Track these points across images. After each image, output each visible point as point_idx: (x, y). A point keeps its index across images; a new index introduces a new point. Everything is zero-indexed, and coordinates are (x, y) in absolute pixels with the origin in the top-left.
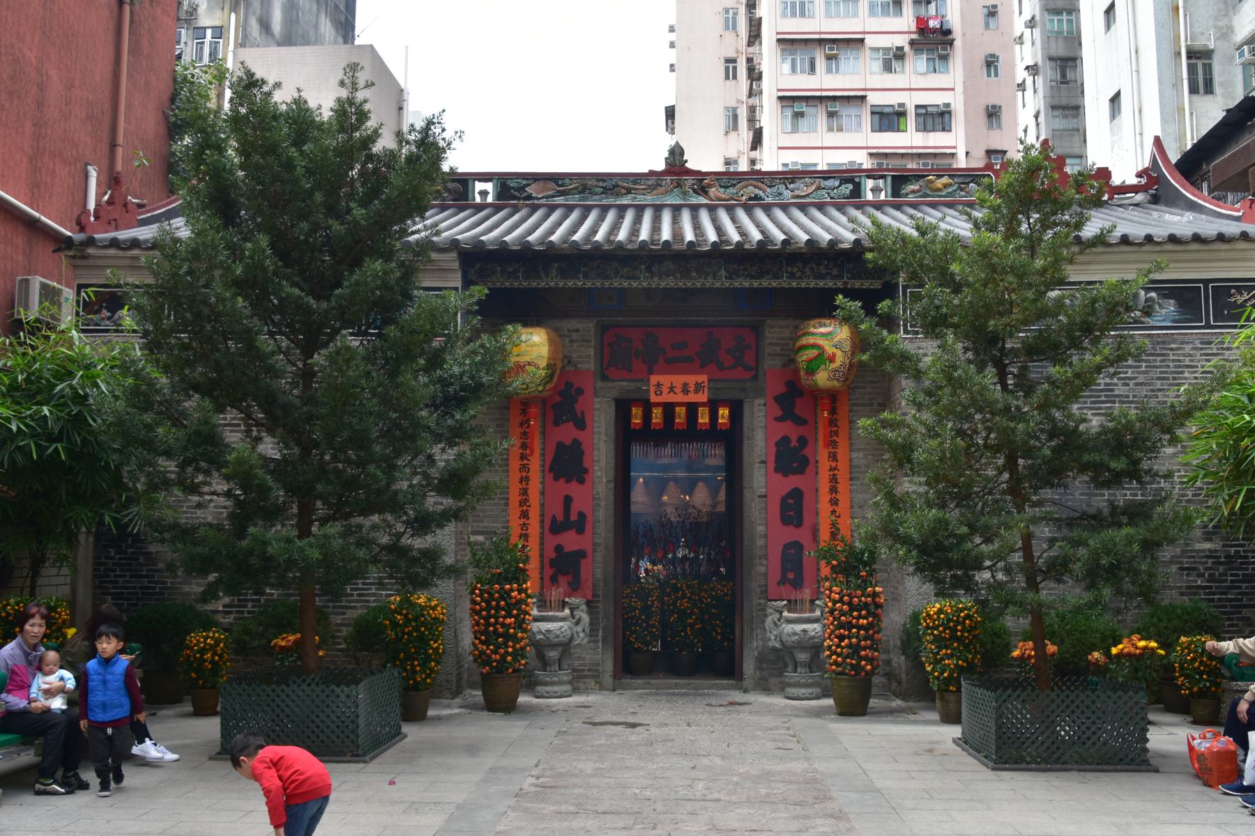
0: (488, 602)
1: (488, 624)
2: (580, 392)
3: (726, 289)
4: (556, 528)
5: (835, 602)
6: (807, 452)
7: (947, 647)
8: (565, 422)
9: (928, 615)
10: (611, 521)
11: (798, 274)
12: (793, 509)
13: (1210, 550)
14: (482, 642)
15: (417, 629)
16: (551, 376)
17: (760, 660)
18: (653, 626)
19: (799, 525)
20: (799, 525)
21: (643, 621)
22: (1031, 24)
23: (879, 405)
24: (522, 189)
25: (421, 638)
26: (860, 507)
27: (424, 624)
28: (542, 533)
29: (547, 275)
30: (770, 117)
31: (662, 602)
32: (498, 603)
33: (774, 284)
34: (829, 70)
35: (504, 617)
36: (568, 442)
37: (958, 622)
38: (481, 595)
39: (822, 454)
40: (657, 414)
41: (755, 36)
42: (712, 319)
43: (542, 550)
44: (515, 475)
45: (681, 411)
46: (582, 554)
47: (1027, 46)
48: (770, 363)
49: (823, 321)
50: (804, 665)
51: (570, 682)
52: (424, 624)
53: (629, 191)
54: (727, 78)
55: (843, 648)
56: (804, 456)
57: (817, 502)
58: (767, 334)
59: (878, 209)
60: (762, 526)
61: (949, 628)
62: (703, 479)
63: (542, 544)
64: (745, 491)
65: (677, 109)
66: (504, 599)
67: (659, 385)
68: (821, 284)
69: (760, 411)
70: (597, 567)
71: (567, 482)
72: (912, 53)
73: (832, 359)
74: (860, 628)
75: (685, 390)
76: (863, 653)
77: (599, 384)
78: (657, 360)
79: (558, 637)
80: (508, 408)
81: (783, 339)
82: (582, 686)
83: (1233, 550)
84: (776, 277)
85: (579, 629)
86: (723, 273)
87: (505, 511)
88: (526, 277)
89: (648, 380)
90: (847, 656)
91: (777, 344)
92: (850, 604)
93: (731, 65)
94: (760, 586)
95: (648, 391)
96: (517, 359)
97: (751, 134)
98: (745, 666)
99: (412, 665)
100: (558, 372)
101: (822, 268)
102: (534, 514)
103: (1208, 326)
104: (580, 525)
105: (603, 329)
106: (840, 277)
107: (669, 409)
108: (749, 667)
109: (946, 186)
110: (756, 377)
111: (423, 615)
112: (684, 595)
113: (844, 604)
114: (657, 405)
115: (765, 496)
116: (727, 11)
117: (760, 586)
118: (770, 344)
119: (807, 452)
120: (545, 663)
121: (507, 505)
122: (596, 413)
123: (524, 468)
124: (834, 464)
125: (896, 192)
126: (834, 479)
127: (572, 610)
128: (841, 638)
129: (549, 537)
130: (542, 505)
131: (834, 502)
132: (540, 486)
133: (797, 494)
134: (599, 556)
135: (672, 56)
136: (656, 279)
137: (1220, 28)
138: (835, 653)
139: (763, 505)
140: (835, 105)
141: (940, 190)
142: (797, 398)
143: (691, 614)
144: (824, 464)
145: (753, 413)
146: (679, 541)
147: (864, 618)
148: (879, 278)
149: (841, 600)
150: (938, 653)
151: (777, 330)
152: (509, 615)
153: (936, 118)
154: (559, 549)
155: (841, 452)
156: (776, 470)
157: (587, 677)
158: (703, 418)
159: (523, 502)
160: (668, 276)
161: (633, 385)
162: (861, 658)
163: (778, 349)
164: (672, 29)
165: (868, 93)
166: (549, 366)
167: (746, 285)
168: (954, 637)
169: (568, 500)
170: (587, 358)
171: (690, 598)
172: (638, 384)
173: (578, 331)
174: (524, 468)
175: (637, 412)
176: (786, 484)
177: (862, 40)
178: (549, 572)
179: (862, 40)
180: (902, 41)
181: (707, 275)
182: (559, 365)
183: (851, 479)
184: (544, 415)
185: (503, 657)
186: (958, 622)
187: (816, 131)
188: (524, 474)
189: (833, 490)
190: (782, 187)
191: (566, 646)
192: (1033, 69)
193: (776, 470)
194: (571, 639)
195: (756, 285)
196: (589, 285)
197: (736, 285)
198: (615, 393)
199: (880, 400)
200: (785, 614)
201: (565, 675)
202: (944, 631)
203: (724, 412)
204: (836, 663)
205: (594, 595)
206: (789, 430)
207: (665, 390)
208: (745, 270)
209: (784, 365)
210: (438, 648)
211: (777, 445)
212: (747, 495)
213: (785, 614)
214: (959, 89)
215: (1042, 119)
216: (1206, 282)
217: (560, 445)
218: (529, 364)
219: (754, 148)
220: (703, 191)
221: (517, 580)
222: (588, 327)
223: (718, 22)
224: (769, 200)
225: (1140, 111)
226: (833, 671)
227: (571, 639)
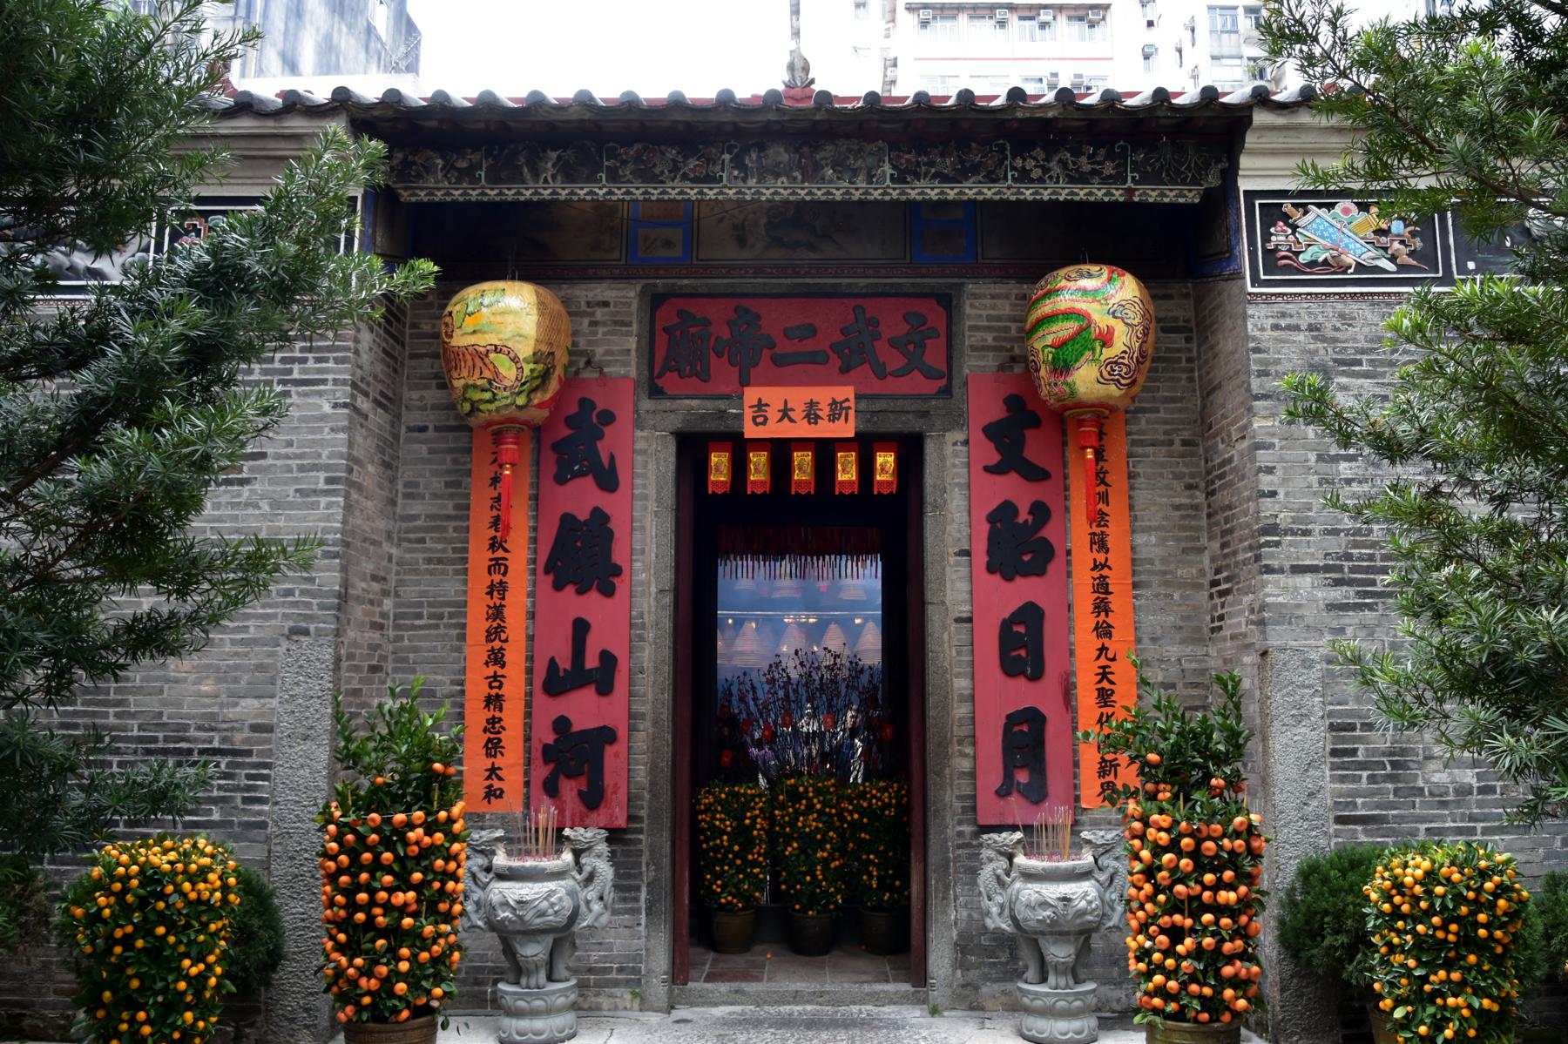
0: (354, 854)
1: (353, 907)
2: (608, 418)
3: (894, 203)
4: (556, 683)
5: (1158, 850)
6: (1048, 533)
7: (1449, 965)
8: (577, 475)
9: (1398, 886)
10: (667, 669)
12: (1022, 645)
14: (340, 948)
15: (145, 930)
16: (545, 376)
17: (965, 947)
18: (755, 864)
19: (1036, 675)
20: (1036, 675)
21: (736, 855)
23: (1185, 443)
25: (156, 952)
26: (1154, 640)
27: (162, 918)
28: (530, 694)
29: (536, 174)
31: (772, 820)
32: (377, 856)
33: (989, 194)
35: (391, 890)
36: (583, 514)
37: (1477, 905)
38: (338, 838)
39: (1075, 533)
40: (758, 461)
42: (863, 282)
43: (528, 727)
44: (480, 579)
45: (803, 461)
46: (606, 735)
48: (976, 365)
49: (1085, 267)
50: (1061, 970)
51: (574, 1007)
52: (162, 918)
55: (1179, 958)
56: (1045, 541)
57: (1070, 630)
58: (968, 310)
60: (964, 677)
61: (1458, 919)
62: (836, 620)
63: (528, 715)
64: (930, 609)
66: (390, 846)
67: (760, 405)
68: (1081, 193)
69: (956, 454)
70: (641, 758)
71: (580, 592)
73: (1106, 339)
74: (1219, 910)
75: (812, 416)
76: (1228, 970)
77: (646, 404)
78: (756, 358)
79: (543, 914)
80: (469, 451)
81: (999, 318)
82: (604, 1002)
84: (992, 178)
85: (591, 893)
86: (888, 169)
87: (459, 650)
88: (494, 179)
89: (741, 397)
90: (1193, 978)
91: (989, 329)
92: (1195, 855)
94: (960, 798)
95: (739, 417)
96: (472, 340)
98: (933, 959)
99: (132, 1021)
100: (559, 371)
101: (1083, 160)
102: (515, 655)
104: (603, 677)
105: (655, 301)
106: (1119, 178)
107: (780, 451)
108: (940, 961)
110: (947, 391)
111: (163, 896)
112: (810, 807)
113: (1180, 854)
114: (759, 444)
115: (970, 620)
117: (960, 798)
118: (974, 328)
119: (1048, 533)
120: (518, 971)
121: (462, 637)
122: (639, 458)
123: (498, 565)
124: (1101, 557)
126: (1102, 586)
127: (577, 854)
128: (1176, 934)
129: (540, 698)
130: (531, 638)
131: (1104, 630)
132: (528, 601)
133: (1031, 615)
134: (641, 740)
136: (752, 182)
138: (1160, 968)
139: (965, 637)
142: (1034, 428)
143: (824, 841)
144: (1083, 558)
145: (943, 459)
146: (802, 708)
147: (1231, 887)
148: (1195, 182)
149: (1174, 846)
150: (1424, 979)
151: (987, 302)
152: (404, 884)
154: (561, 724)
155: (1115, 532)
156: (991, 569)
157: (616, 983)
158: (847, 472)
159: (494, 633)
160: (777, 175)
161: (710, 406)
162: (1222, 982)
163: (989, 338)
166: (537, 357)
167: (933, 195)
168: (1468, 941)
169: (581, 628)
170: (621, 354)
171: (821, 813)
172: (721, 404)
173: (606, 304)
174: (498, 565)
175: (719, 461)
176: (1014, 594)
178: (541, 772)
181: (855, 172)
182: (562, 358)
183: (1135, 586)
184: (538, 463)
185: (387, 982)
186: (1477, 905)
188: (497, 578)
189: (1102, 607)
191: (563, 935)
193: (991, 569)
194: (574, 916)
195: (952, 195)
196: (619, 194)
197: (913, 194)
198: (676, 422)
199: (1186, 435)
200: (1020, 860)
201: (561, 990)
202: (1444, 927)
203: (885, 461)
204: (1160, 991)
205: (631, 818)
206: (1017, 491)
207: (773, 414)
208: (931, 164)
209: (1001, 368)
210: (202, 977)
211: (992, 518)
212: (934, 617)
213: (1020, 860)
217: (568, 521)
218: (497, 349)
221: (424, 800)
222: (626, 296)
226: (1156, 1011)
227: (574, 916)
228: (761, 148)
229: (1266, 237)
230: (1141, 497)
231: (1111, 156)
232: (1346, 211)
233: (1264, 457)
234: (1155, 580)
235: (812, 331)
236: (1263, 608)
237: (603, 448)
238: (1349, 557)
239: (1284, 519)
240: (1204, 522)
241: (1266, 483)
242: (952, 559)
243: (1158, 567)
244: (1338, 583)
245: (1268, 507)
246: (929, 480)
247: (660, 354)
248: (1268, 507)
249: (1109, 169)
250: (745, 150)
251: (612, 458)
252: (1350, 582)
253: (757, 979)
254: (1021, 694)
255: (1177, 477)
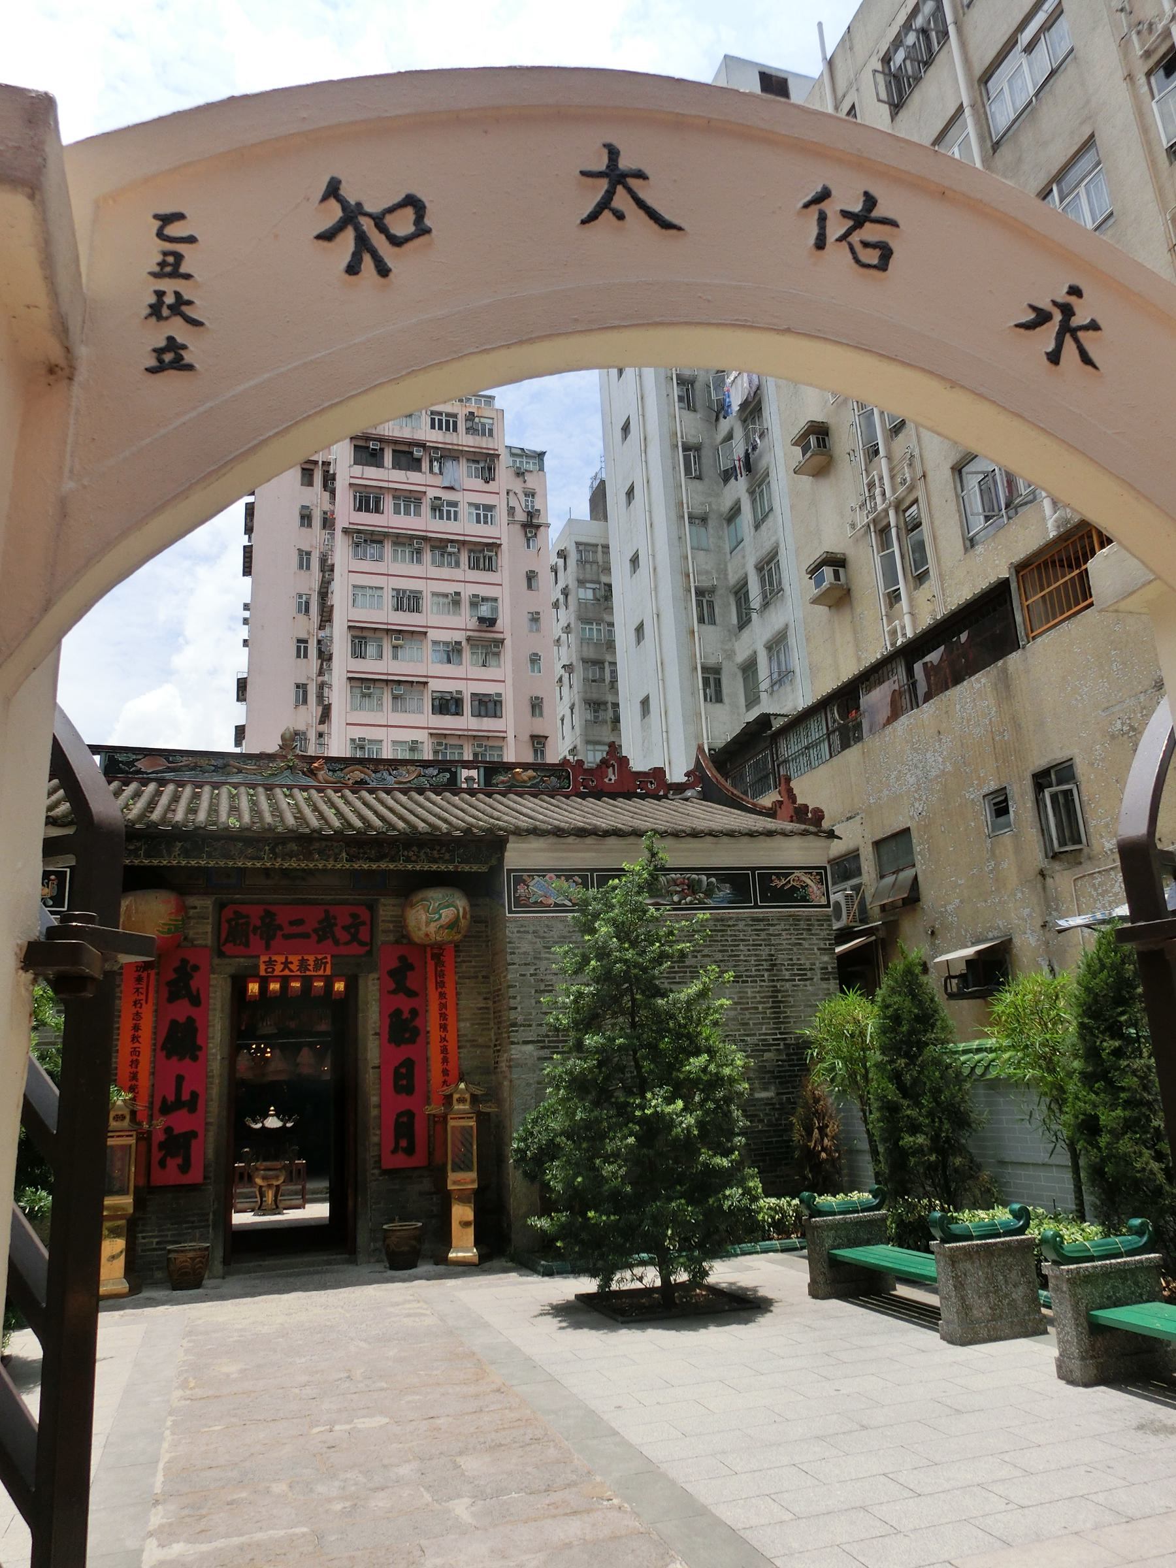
2: (196, 968)
6: (417, 1022)
11: (413, 858)
13: (767, 1099)
22: (567, 629)
24: (131, 763)
30: (339, 695)
34: (395, 657)
36: (181, 1019)
39: (432, 1023)
41: (326, 616)
42: (329, 897)
46: (193, 1135)
47: (564, 650)
53: (240, 771)
54: (298, 656)
56: (416, 1027)
58: (381, 912)
59: (472, 796)
65: (249, 680)
68: (434, 867)
71: (180, 1059)
72: (468, 648)
77: (216, 961)
83: (784, 1097)
84: (393, 860)
86: (344, 855)
88: (147, 856)
91: (389, 922)
93: (452, 509)
97: (320, 709)
103: (756, 906)
105: (221, 906)
106: (452, 861)
109: (530, 779)
110: (370, 953)
116: (300, 596)
119: (417, 1022)
125: (488, 782)
133: (409, 1064)
134: (211, 1135)
135: (244, 632)
137: (725, 651)
140: (402, 689)
141: (525, 782)
142: (411, 965)
153: (488, 705)
163: (391, 926)
164: (246, 607)
165: (429, 680)
169: (180, 1079)
170: (204, 932)
173: (195, 908)
177: (425, 633)
179: (425, 633)
180: (460, 636)
183: (459, 1047)
187: (382, 710)
190: (385, 774)
192: (568, 668)
195: (374, 867)
196: (212, 864)
197: (356, 866)
198: (231, 970)
199: (484, 973)
205: (205, 1178)
208: (365, 853)
214: (509, 682)
215: (576, 710)
216: (753, 869)
217: (174, 1022)
219: (322, 722)
220: (312, 773)
223: (292, 605)
224: (373, 784)
225: (666, 712)
228: (284, 844)
229: (516, 890)
230: (462, 1003)
231: (448, 851)
232: (551, 878)
233: (512, 992)
234: (468, 1044)
235: (300, 922)
236: (511, 1060)
237: (194, 984)
238: (548, 1036)
239: (520, 1019)
240: (492, 1016)
241: (512, 1003)
242: (371, 1038)
243: (470, 1037)
244: (543, 1048)
245: (513, 1015)
246: (361, 993)
247: (223, 936)
248: (513, 1015)
249: (447, 856)
250: (276, 845)
251: (198, 990)
252: (548, 1047)
253: (416, 1266)
254: (405, 1102)
255: (479, 993)
